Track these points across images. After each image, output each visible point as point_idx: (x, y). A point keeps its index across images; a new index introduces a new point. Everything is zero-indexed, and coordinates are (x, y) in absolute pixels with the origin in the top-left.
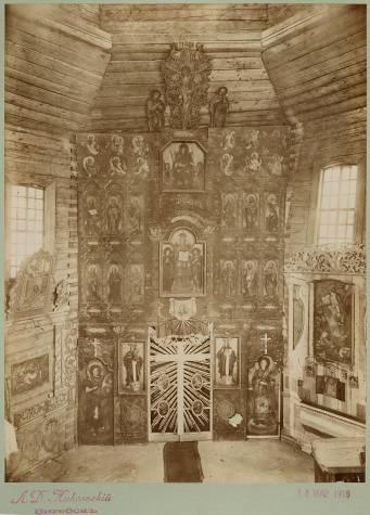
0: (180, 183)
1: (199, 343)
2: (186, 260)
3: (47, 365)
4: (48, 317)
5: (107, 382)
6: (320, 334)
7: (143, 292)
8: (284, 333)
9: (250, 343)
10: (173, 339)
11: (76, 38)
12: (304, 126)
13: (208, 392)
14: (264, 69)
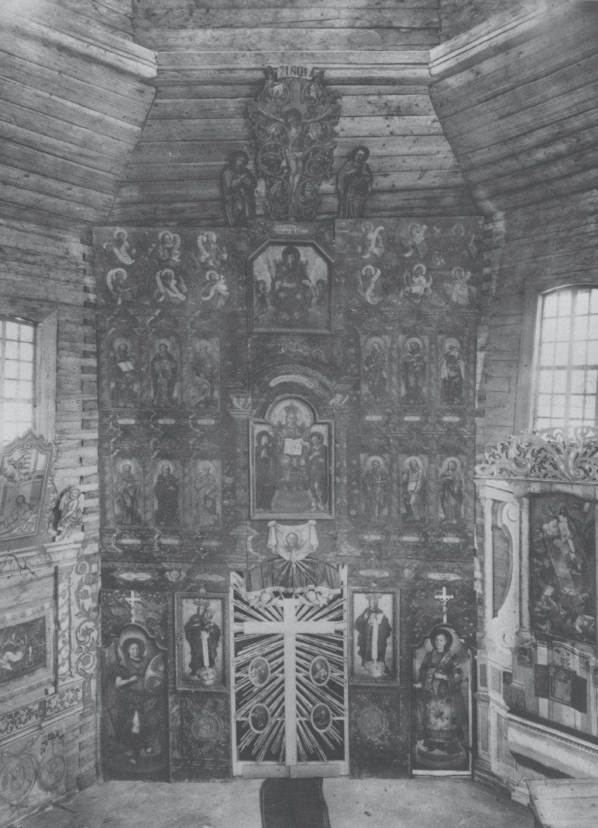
0: (285, 316)
1: (323, 601)
2: (298, 452)
3: (42, 635)
4: (43, 551)
5: (155, 669)
6: (541, 591)
7: (219, 508)
8: (478, 588)
9: (415, 604)
10: (276, 594)
11: (89, 59)
12: (507, 217)
13: (340, 690)
14: (434, 116)
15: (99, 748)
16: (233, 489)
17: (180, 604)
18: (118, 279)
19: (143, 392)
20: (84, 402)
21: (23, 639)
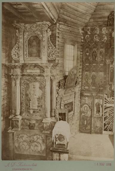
3: (72, 105)
5: (89, 112)
7: (103, 82)
16: (106, 78)
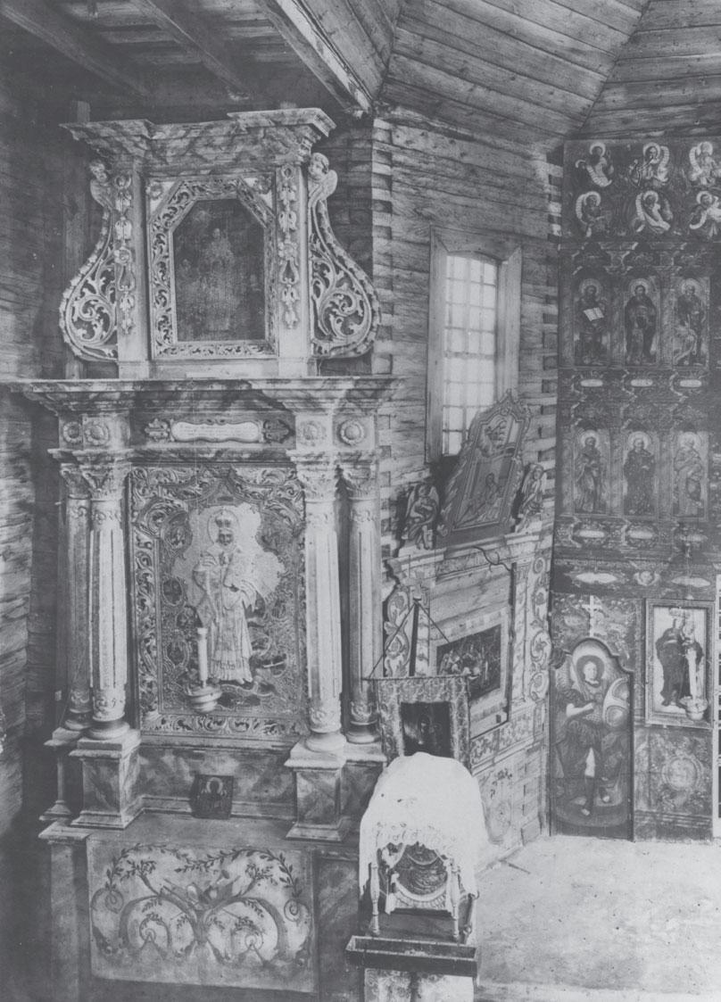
3: (497, 649)
5: (616, 695)
7: (704, 494)
15: (544, 793)
17: (652, 614)
18: (589, 205)
19: (613, 345)
20: (545, 359)
21: (480, 651)
